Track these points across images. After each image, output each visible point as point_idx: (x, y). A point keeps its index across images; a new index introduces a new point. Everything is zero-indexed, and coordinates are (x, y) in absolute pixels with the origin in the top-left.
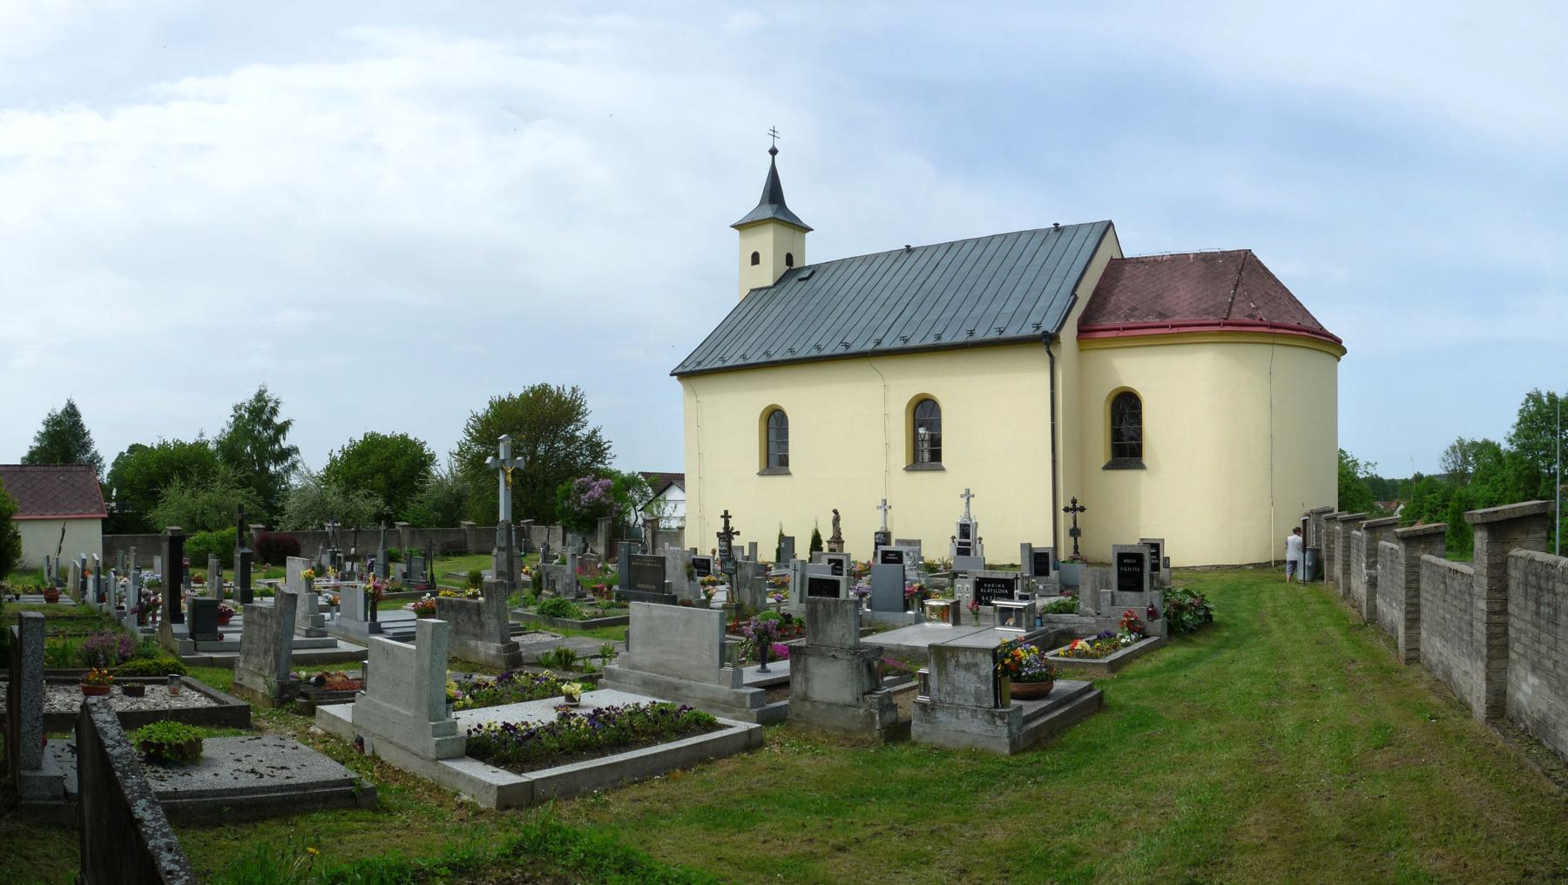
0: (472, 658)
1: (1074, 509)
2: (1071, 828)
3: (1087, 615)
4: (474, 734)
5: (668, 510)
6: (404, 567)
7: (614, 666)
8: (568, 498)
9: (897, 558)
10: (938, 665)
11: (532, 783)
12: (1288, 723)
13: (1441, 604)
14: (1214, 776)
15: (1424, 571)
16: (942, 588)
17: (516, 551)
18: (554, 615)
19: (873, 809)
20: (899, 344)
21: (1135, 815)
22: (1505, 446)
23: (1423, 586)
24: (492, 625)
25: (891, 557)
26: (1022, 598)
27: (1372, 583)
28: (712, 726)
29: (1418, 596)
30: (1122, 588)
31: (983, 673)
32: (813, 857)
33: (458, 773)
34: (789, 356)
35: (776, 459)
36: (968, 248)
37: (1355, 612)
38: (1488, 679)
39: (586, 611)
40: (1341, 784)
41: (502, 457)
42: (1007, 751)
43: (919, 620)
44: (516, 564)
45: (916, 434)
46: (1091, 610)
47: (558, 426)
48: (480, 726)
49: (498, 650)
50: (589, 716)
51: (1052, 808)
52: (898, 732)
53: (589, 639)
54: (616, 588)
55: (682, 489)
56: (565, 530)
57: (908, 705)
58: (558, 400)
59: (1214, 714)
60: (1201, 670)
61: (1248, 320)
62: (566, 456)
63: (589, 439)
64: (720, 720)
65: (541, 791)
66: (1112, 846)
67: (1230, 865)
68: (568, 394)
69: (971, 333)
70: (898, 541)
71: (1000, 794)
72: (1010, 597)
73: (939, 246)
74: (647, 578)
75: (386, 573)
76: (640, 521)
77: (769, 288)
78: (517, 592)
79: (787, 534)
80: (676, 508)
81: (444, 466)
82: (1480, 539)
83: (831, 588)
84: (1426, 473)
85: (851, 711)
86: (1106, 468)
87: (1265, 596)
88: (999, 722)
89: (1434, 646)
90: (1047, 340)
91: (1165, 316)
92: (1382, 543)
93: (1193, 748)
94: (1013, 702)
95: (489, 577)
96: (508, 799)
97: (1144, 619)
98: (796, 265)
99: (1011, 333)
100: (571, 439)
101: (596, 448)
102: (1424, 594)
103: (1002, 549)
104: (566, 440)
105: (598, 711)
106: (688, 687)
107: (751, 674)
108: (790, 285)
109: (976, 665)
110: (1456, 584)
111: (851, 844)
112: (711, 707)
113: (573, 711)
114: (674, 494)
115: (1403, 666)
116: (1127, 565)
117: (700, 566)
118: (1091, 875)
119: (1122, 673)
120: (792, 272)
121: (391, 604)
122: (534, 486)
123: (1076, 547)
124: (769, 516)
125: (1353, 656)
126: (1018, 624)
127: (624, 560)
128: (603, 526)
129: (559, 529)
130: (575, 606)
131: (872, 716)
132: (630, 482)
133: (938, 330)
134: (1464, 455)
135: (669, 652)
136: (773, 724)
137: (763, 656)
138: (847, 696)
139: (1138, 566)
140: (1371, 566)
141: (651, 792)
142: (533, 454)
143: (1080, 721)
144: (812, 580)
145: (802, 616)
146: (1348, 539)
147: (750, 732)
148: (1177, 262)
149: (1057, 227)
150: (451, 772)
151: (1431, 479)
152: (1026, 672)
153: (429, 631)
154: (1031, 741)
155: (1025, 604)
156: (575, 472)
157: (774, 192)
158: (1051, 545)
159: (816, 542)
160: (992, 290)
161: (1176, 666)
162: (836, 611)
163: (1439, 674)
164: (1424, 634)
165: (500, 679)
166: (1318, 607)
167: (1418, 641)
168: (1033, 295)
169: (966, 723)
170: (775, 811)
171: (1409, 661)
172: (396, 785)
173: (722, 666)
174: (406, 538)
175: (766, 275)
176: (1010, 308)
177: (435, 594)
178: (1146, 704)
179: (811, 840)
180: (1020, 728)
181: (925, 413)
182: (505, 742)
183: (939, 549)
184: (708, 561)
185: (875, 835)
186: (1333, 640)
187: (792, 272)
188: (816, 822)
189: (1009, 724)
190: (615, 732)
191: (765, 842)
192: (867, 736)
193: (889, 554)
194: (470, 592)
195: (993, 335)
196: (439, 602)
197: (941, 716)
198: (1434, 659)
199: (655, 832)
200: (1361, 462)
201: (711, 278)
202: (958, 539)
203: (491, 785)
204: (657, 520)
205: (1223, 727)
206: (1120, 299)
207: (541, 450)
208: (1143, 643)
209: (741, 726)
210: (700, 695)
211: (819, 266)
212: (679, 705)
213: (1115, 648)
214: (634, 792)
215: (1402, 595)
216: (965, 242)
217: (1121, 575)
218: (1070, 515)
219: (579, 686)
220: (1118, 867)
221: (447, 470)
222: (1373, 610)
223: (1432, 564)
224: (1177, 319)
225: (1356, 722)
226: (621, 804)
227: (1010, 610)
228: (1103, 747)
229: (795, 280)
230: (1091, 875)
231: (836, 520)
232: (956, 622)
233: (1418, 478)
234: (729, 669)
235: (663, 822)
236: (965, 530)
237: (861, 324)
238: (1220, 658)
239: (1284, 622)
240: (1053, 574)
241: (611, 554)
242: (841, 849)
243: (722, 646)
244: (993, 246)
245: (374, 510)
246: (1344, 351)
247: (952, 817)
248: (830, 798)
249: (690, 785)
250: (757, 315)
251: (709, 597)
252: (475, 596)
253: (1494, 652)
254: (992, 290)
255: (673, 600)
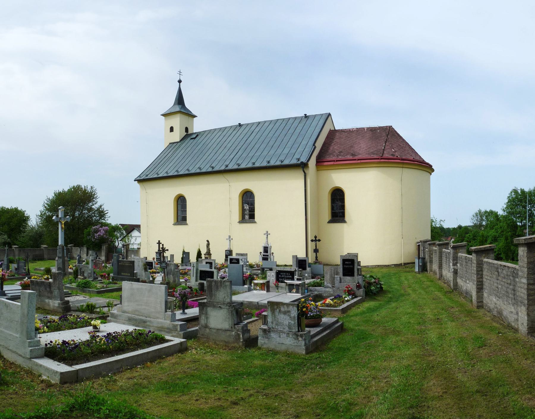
0: (47, 308)
1: (316, 240)
2: (344, 391)
3: (328, 287)
4: (48, 346)
5: (133, 241)
6: (15, 266)
7: (115, 311)
8: (89, 235)
9: (237, 261)
10: (271, 311)
11: (77, 371)
12: (433, 335)
13: (496, 281)
14: (405, 362)
15: (485, 266)
16: (257, 275)
17: (66, 258)
18: (84, 287)
19: (246, 382)
20: (236, 167)
21: (373, 383)
22: (501, 213)
23: (485, 273)
24: (56, 292)
25: (234, 261)
26: (298, 279)
27: (455, 272)
28: (163, 340)
29: (482, 278)
30: (344, 275)
31: (292, 315)
32: (222, 408)
33: (41, 365)
34: (187, 172)
35: (181, 218)
36: (267, 124)
37: (446, 285)
38: (528, 315)
39: (99, 285)
40: (469, 364)
41: (60, 216)
42: (304, 352)
43: (250, 290)
44: (66, 264)
45: (243, 207)
46: (330, 285)
47: (85, 203)
48: (51, 342)
49: (59, 304)
50: (105, 336)
51: (332, 380)
52: (251, 342)
53: (101, 298)
54: (112, 275)
55: (140, 232)
56: (88, 249)
57: (256, 328)
58: (85, 192)
59: (396, 332)
60: (383, 312)
61: (391, 157)
62: (88, 217)
63: (98, 209)
64: (167, 337)
65: (81, 374)
66: (367, 400)
67: (429, 407)
68: (89, 189)
69: (269, 162)
70: (237, 254)
71: (305, 374)
72: (293, 279)
73: (253, 124)
74: (126, 270)
75: (8, 268)
76: (120, 245)
77: (178, 142)
78: (67, 277)
79: (186, 251)
80: (136, 240)
81: (34, 221)
82: (522, 252)
83: (210, 274)
84: (463, 225)
85: (228, 333)
86: (329, 222)
87: (403, 279)
88: (300, 339)
89: (491, 300)
90: (303, 166)
91: (355, 155)
92: (460, 254)
93: (391, 349)
94: (306, 329)
95: (54, 270)
96: (65, 378)
97: (355, 289)
98: (190, 132)
99: (286, 162)
100: (91, 209)
101: (101, 213)
102: (485, 277)
103: (284, 257)
104: (88, 209)
105: (109, 334)
106: (150, 321)
107: (179, 315)
108: (187, 141)
109: (289, 312)
110: (504, 272)
111: (239, 400)
112: (160, 331)
113: (98, 334)
114: (135, 233)
115: (476, 310)
116: (347, 264)
117: (149, 265)
118: (362, 415)
119: (347, 314)
120: (188, 135)
121: (10, 282)
122: (74, 230)
123: (316, 257)
124: (180, 242)
125: (451, 305)
126: (297, 292)
127: (116, 262)
128: (104, 248)
129: (85, 249)
130: (94, 283)
131: (239, 335)
132: (115, 229)
133: (253, 161)
134: (481, 216)
135: (141, 304)
136: (191, 339)
137: (184, 307)
138: (226, 325)
139: (350, 265)
140: (455, 264)
141: (136, 374)
142: (73, 216)
143: (334, 337)
144: (201, 271)
145: (197, 287)
146: (441, 253)
147: (181, 343)
148: (359, 131)
149: (306, 116)
150: (37, 365)
151: (466, 228)
152: (310, 314)
153: (27, 296)
154: (314, 347)
155: (300, 282)
156: (91, 224)
157: (180, 100)
158: (305, 256)
159: (199, 254)
160: (277, 143)
161: (371, 310)
162: (221, 285)
163: (495, 313)
164: (485, 295)
165: (60, 319)
166: (429, 283)
167: (482, 298)
168: (296, 146)
169: (284, 339)
170: (198, 383)
171: (478, 307)
172: (11, 371)
173: (166, 311)
174: (17, 252)
175: (176, 136)
176: (286, 151)
177: (30, 278)
178: (363, 328)
179: (219, 399)
180: (309, 341)
181: (247, 198)
182: (64, 350)
183: (255, 258)
184: (152, 263)
185: (251, 396)
186: (440, 298)
187: (188, 135)
188: (220, 389)
189: (305, 340)
190: (118, 344)
191: (197, 400)
192: (236, 345)
193: (232, 259)
194: (46, 277)
195: (278, 163)
196: (32, 281)
197: (272, 334)
198: (492, 306)
199: (141, 396)
200: (438, 220)
201: (156, 137)
202: (263, 253)
203: (57, 372)
204: (128, 245)
205: (403, 339)
206: (335, 147)
207: (77, 214)
208: (355, 300)
209: (177, 340)
210: (155, 325)
211: (200, 133)
212: (147, 330)
213: (343, 302)
214: (128, 374)
215: (475, 277)
216: (265, 122)
217: (344, 269)
218: (314, 243)
219: (99, 321)
220: (373, 410)
221: (35, 223)
222: (456, 284)
223: (490, 263)
224: (360, 157)
225: (465, 335)
226: (122, 380)
227: (293, 285)
228: (348, 349)
229: (189, 139)
230: (362, 415)
231: (208, 245)
232: (268, 291)
233: (460, 227)
234: (169, 313)
235: (145, 390)
236: (266, 249)
237: (219, 158)
238: (390, 306)
239: (414, 290)
240: (308, 269)
241: (107, 260)
242: (235, 403)
243: (166, 302)
244: (278, 124)
245: (3, 241)
246: (433, 170)
247: (284, 387)
248: (224, 376)
249: (156, 371)
250: (173, 154)
251: (154, 279)
252: (48, 279)
253: (531, 302)
254: (277, 143)
255: (138, 280)
